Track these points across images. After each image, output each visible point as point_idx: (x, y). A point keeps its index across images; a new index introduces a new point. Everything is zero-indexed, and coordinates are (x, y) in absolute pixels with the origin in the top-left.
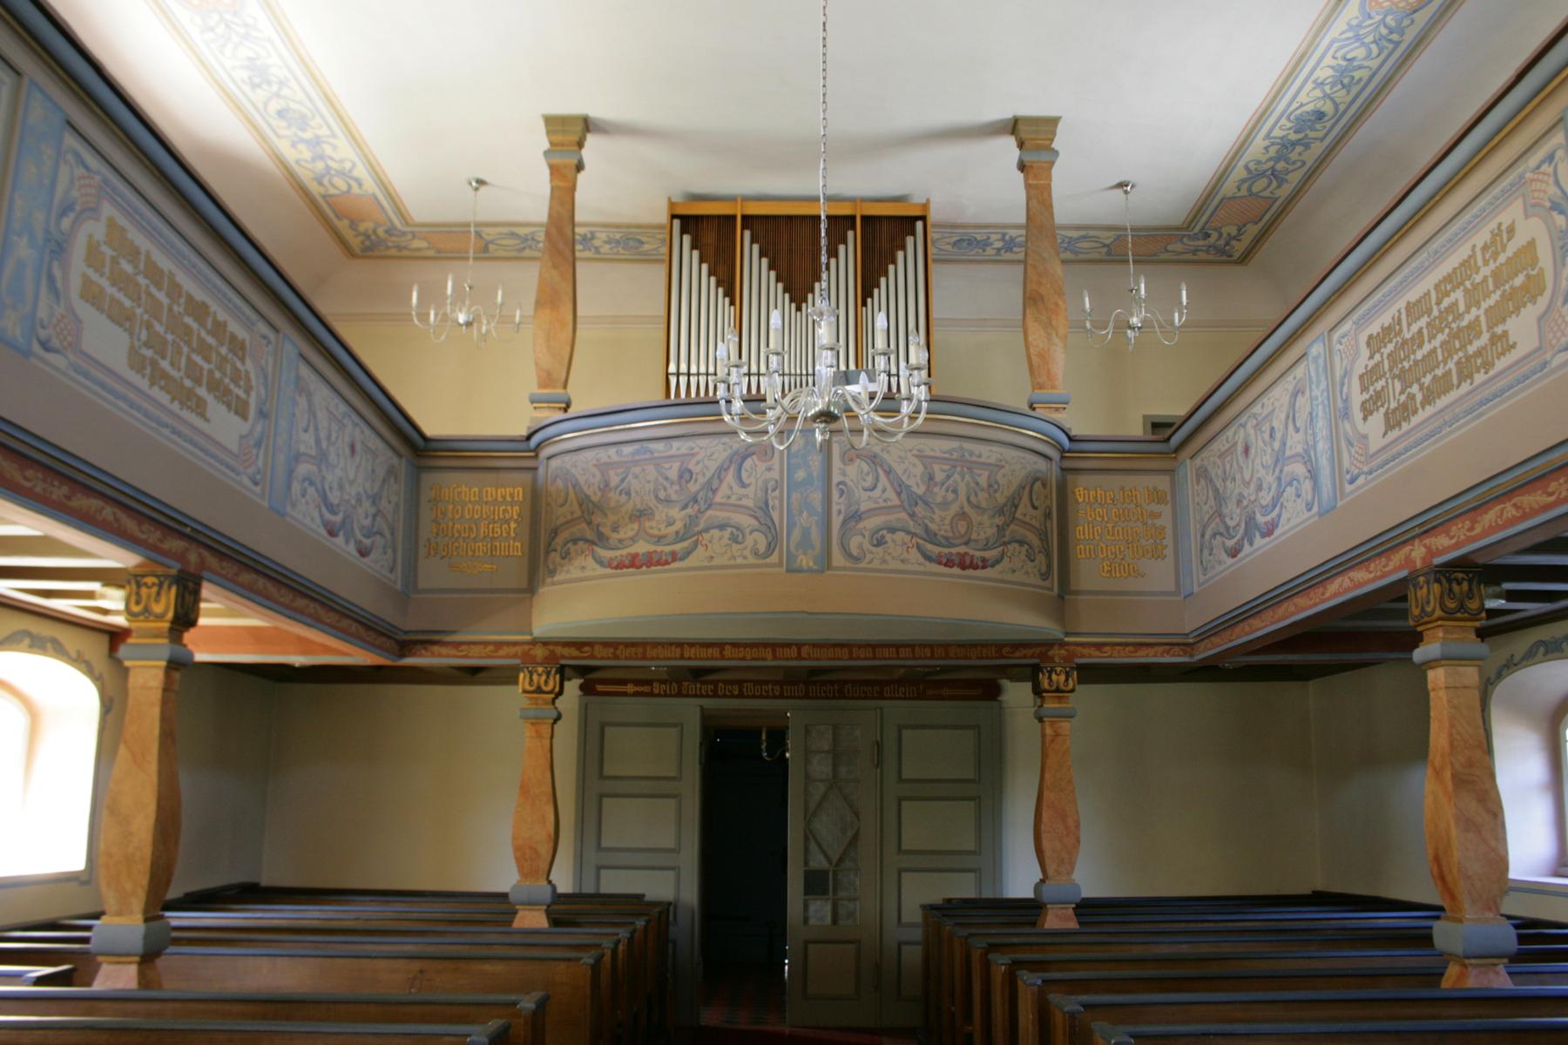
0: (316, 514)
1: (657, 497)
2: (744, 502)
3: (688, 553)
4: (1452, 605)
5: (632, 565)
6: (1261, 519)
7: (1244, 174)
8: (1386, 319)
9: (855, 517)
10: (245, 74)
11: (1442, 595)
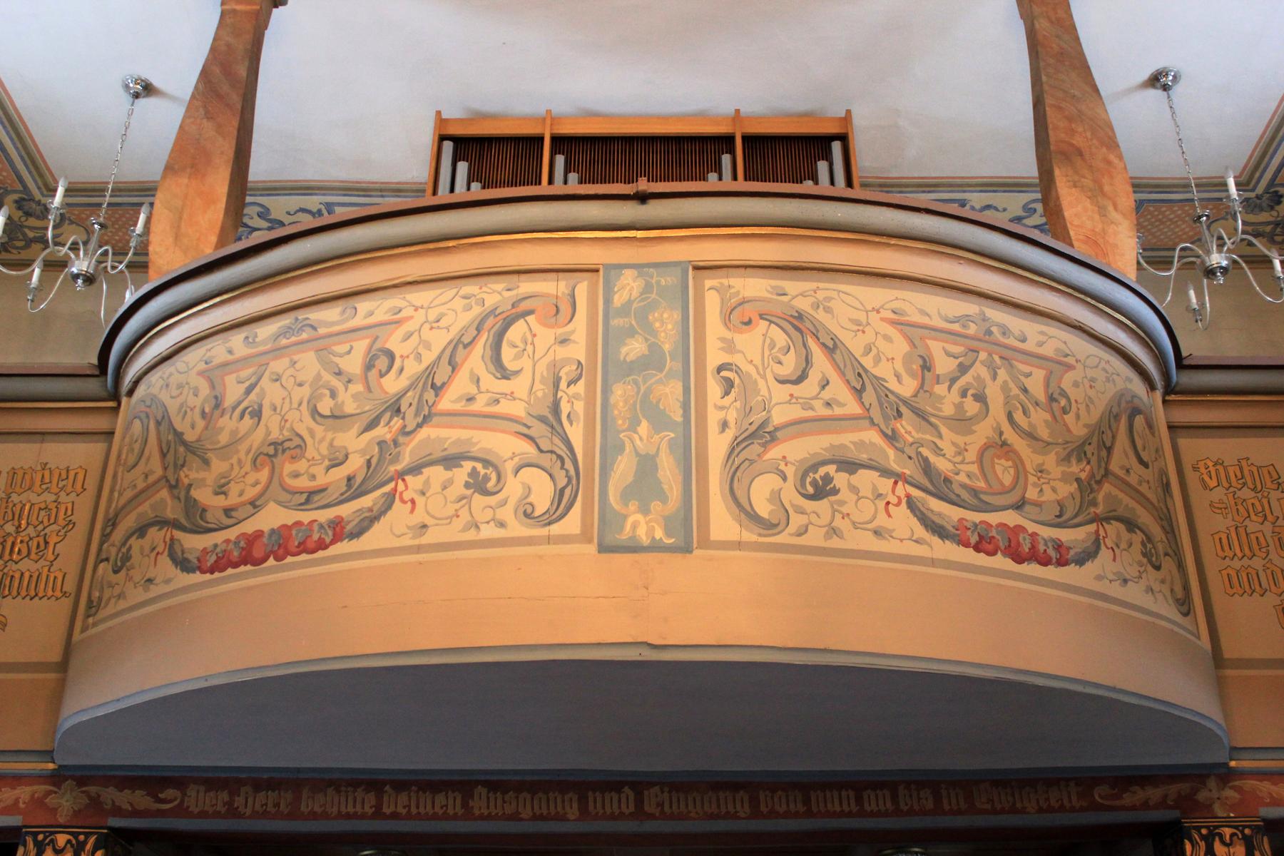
1: (315, 412)
2: (505, 407)
3: (369, 520)
9: (760, 435)
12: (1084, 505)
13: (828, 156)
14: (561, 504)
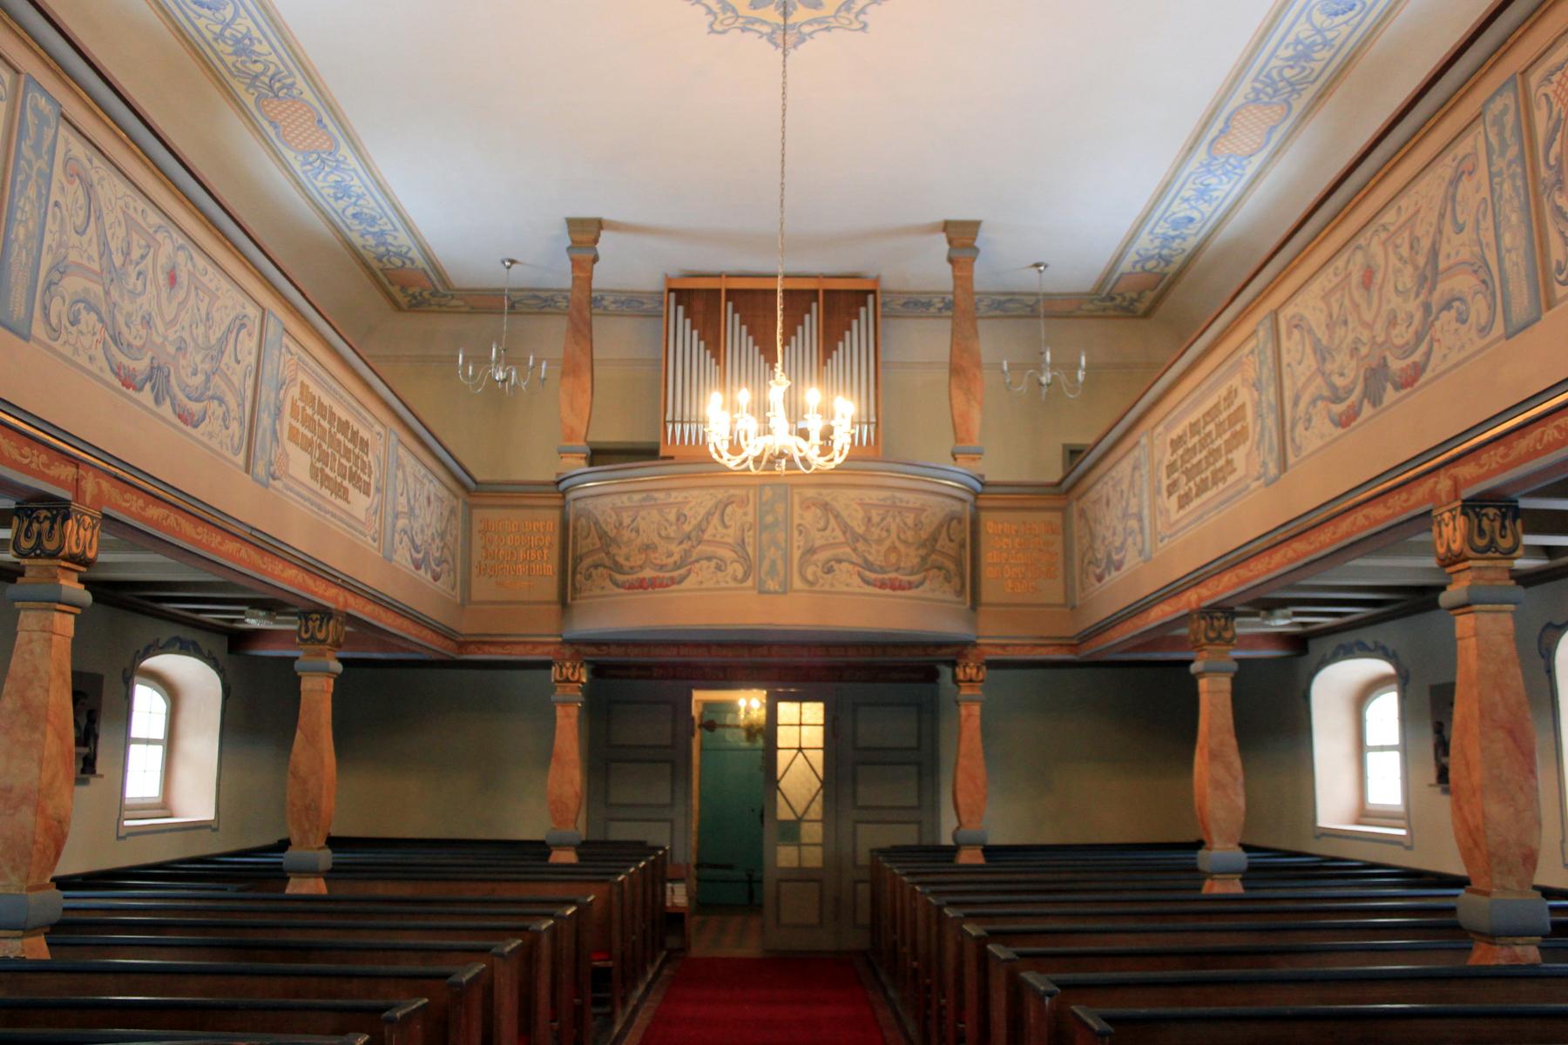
0: (99, 353)
3: (683, 579)
4: (1212, 635)
5: (641, 587)
6: (1396, 365)
7: (1136, 258)
8: (1208, 404)
10: (331, 191)
11: (1470, 531)
12: (924, 566)
13: (865, 304)
14: (746, 576)
